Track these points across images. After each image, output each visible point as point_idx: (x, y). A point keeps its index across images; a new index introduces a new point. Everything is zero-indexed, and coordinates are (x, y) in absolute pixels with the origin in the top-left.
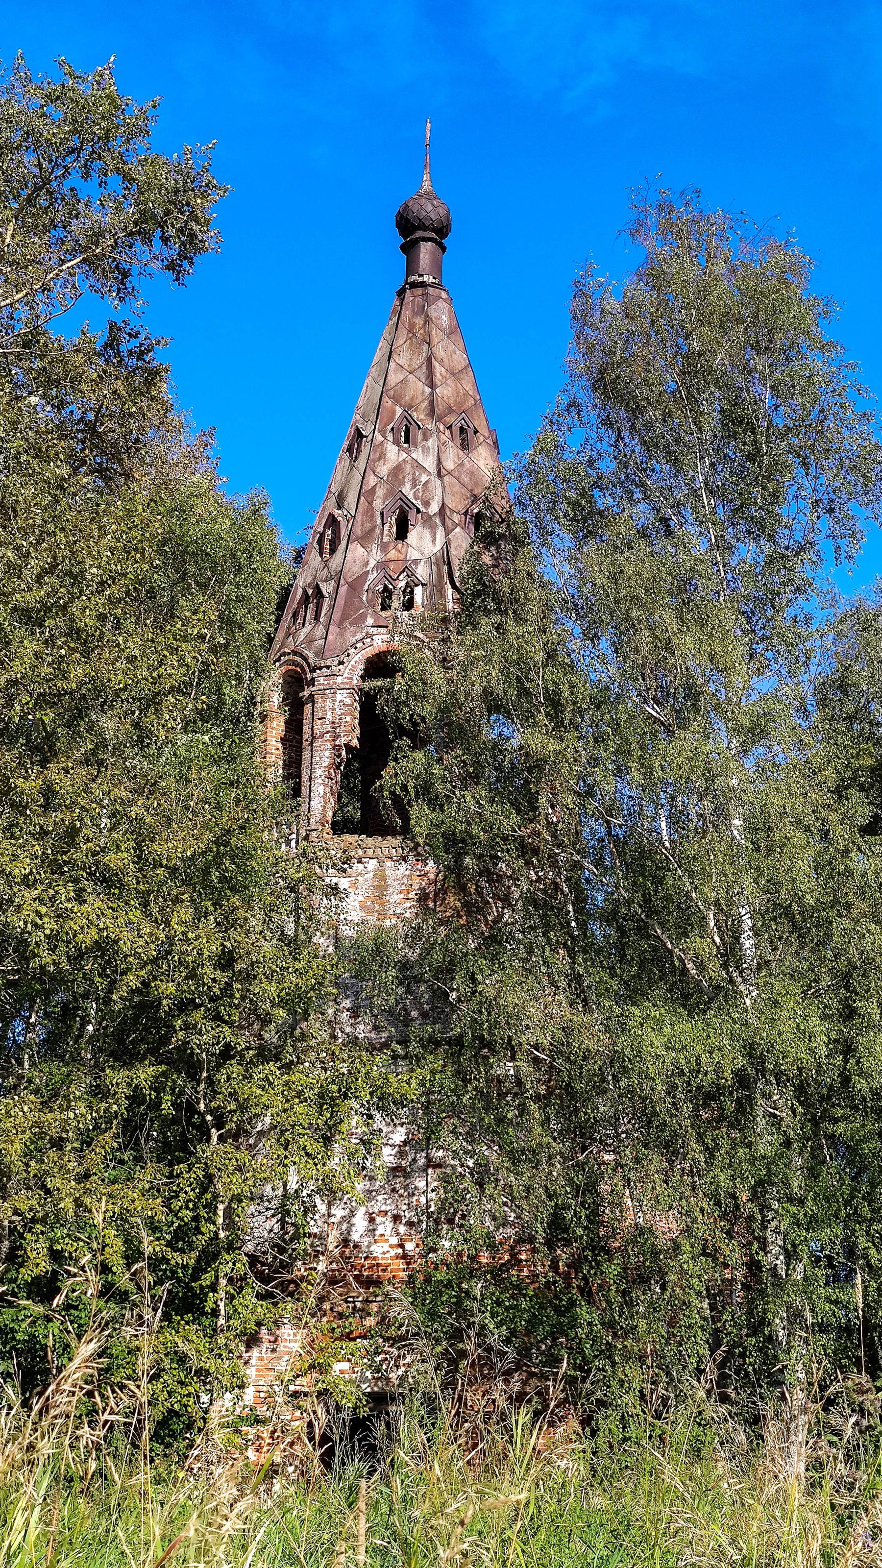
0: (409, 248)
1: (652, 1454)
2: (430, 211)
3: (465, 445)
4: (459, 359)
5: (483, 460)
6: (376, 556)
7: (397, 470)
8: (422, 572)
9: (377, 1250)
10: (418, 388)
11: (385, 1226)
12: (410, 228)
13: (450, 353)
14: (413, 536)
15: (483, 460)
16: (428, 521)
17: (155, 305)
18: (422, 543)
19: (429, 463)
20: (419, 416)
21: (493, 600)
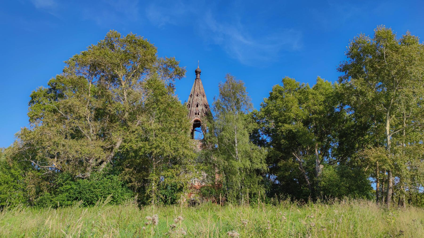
0: (196, 74)
1: (72, 131)
2: (199, 70)
3: (204, 97)
4: (202, 87)
5: (205, 99)
6: (195, 109)
7: (197, 99)
8: (200, 111)
9: (196, 184)
10: (198, 90)
11: (196, 182)
12: (196, 72)
13: (201, 86)
14: (199, 107)
15: (205, 99)
16: (200, 105)
17: (176, 82)
18: (200, 108)
19: (200, 99)
20: (199, 93)
21: (129, 155)
